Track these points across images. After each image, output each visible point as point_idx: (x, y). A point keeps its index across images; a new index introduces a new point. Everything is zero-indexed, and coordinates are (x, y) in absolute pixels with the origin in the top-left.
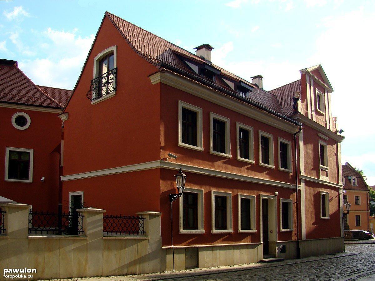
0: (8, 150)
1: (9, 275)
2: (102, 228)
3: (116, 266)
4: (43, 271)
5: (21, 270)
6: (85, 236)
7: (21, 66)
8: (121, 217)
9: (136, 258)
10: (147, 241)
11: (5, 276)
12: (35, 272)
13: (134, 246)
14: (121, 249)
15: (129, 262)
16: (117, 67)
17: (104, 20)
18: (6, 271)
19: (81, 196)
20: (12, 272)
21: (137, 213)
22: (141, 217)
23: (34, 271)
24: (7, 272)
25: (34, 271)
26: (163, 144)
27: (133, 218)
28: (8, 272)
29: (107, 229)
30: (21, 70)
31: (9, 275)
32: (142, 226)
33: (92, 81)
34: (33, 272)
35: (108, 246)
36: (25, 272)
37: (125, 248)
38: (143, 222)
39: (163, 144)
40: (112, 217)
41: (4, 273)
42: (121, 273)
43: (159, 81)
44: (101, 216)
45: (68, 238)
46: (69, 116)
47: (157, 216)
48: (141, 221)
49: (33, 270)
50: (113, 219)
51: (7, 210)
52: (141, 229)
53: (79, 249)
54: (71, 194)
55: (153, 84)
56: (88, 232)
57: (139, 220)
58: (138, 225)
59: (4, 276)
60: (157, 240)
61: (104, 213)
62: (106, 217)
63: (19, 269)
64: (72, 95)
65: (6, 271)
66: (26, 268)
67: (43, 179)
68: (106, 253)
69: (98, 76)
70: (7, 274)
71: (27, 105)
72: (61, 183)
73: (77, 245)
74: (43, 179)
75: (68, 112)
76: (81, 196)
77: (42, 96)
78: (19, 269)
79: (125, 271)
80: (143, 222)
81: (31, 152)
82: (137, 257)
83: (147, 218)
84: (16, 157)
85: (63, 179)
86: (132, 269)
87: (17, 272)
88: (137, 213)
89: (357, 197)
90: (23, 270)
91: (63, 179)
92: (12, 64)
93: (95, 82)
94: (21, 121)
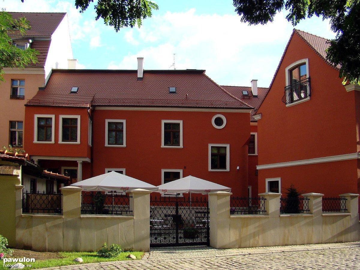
0: (210, 146)
1: (8, 265)
2: (321, 207)
3: (329, 236)
4: (288, 240)
5: (20, 259)
6: (312, 214)
7: (206, 73)
8: (331, 199)
9: (343, 230)
10: (349, 216)
11: (5, 265)
12: (34, 261)
13: (341, 221)
14: (333, 223)
15: (338, 233)
16: (310, 77)
17: (292, 35)
18: (6, 260)
19: (278, 181)
20: (11, 261)
21: (339, 195)
22: (263, 198)
23: (33, 260)
24: (6, 261)
25: (33, 260)
26: (358, 140)
27: (337, 199)
28: (8, 262)
29: (325, 209)
30: (210, 77)
31: (8, 265)
32: (264, 206)
33: (285, 87)
34: (31, 261)
35: (325, 221)
36: (24, 261)
37: (336, 222)
38: (265, 202)
39: (358, 140)
40: (329, 199)
41: (4, 263)
42: (333, 241)
43: (354, 89)
44: (320, 199)
45: (302, 216)
46: (262, 116)
47: (356, 197)
48: (263, 202)
49: (32, 259)
50: (123, 198)
51: (133, 195)
52: (263, 208)
53: (308, 224)
54: (267, 180)
55: (348, 91)
56: (314, 211)
57: (261, 200)
58: (339, 204)
59: (4, 265)
60: (356, 215)
61: (231, 196)
62: (324, 199)
63: (18, 259)
64: (265, 98)
65: (6, 260)
66: (25, 258)
67: (238, 168)
68: (324, 226)
69: (290, 84)
70: (6, 263)
71: (223, 108)
72: (257, 170)
73: (308, 220)
74: (238, 168)
75: (261, 113)
76: (278, 181)
77: (234, 100)
78: (18, 259)
79: (336, 240)
80: (265, 202)
81: (228, 146)
82: (343, 229)
83: (349, 199)
84: (216, 152)
85: (259, 168)
86: (340, 238)
87: (17, 261)
88: (339, 195)
89: (218, 148)
90: (22, 259)
91: (259, 168)
92: (200, 73)
93: (288, 89)
94: (219, 122)
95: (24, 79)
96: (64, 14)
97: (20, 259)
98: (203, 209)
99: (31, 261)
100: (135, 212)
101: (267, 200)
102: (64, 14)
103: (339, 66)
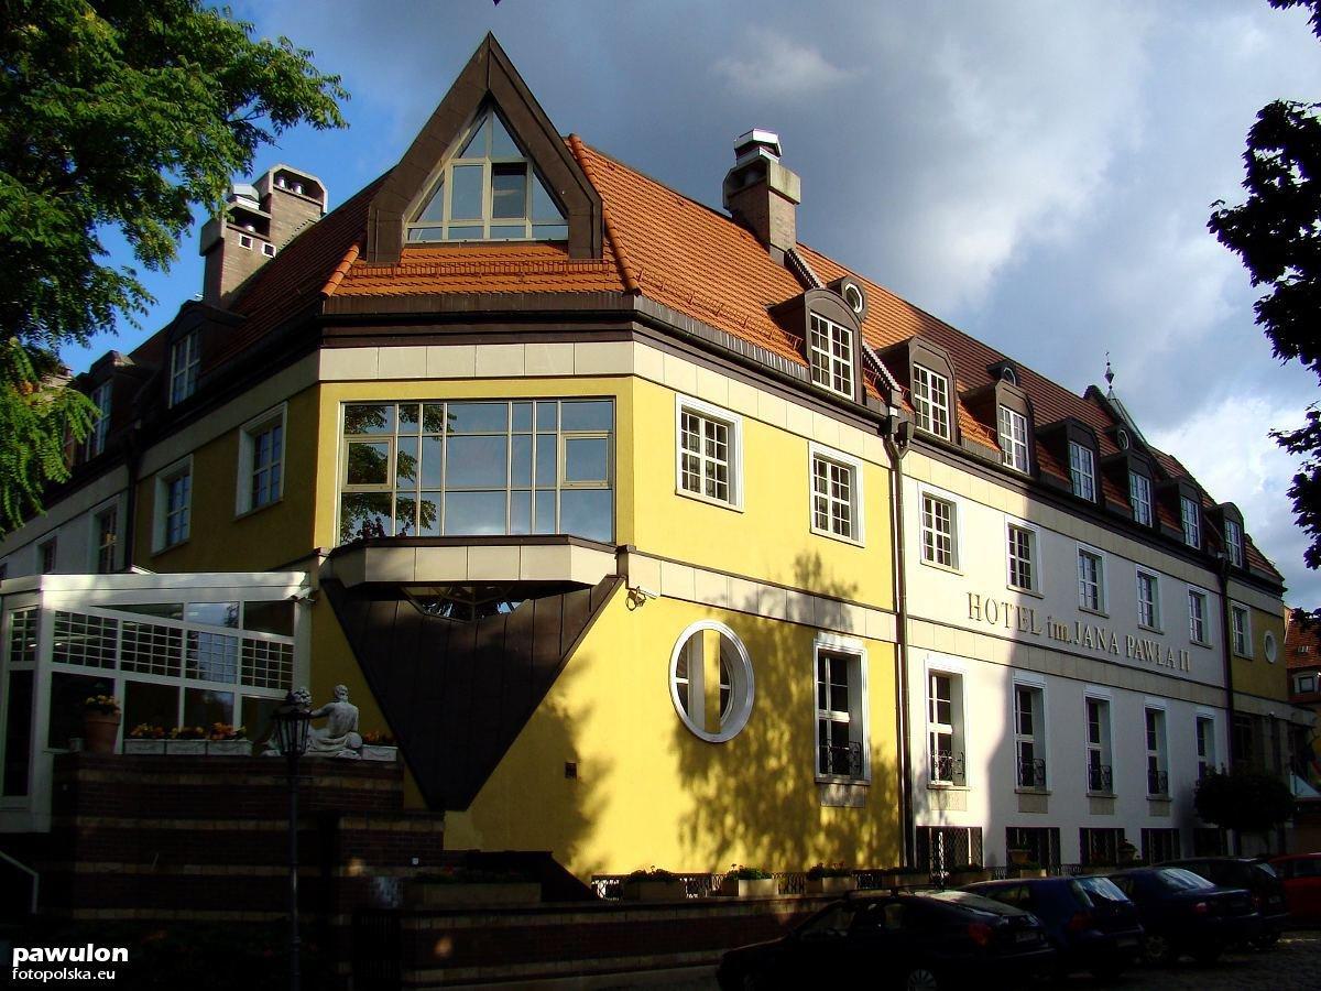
18: (21, 954)
20: (41, 959)
24: (24, 959)
34: (115, 959)
49: (116, 951)
63: (65, 950)
65: (21, 954)
66: (90, 946)
70: (25, 966)
78: (65, 950)
90: (82, 950)
95: (932, 734)
96: (490, 36)
97: (73, 950)
98: (119, 560)
99: (115, 959)
100: (792, 560)
101: (860, 587)
102: (490, 36)
103: (356, 868)
